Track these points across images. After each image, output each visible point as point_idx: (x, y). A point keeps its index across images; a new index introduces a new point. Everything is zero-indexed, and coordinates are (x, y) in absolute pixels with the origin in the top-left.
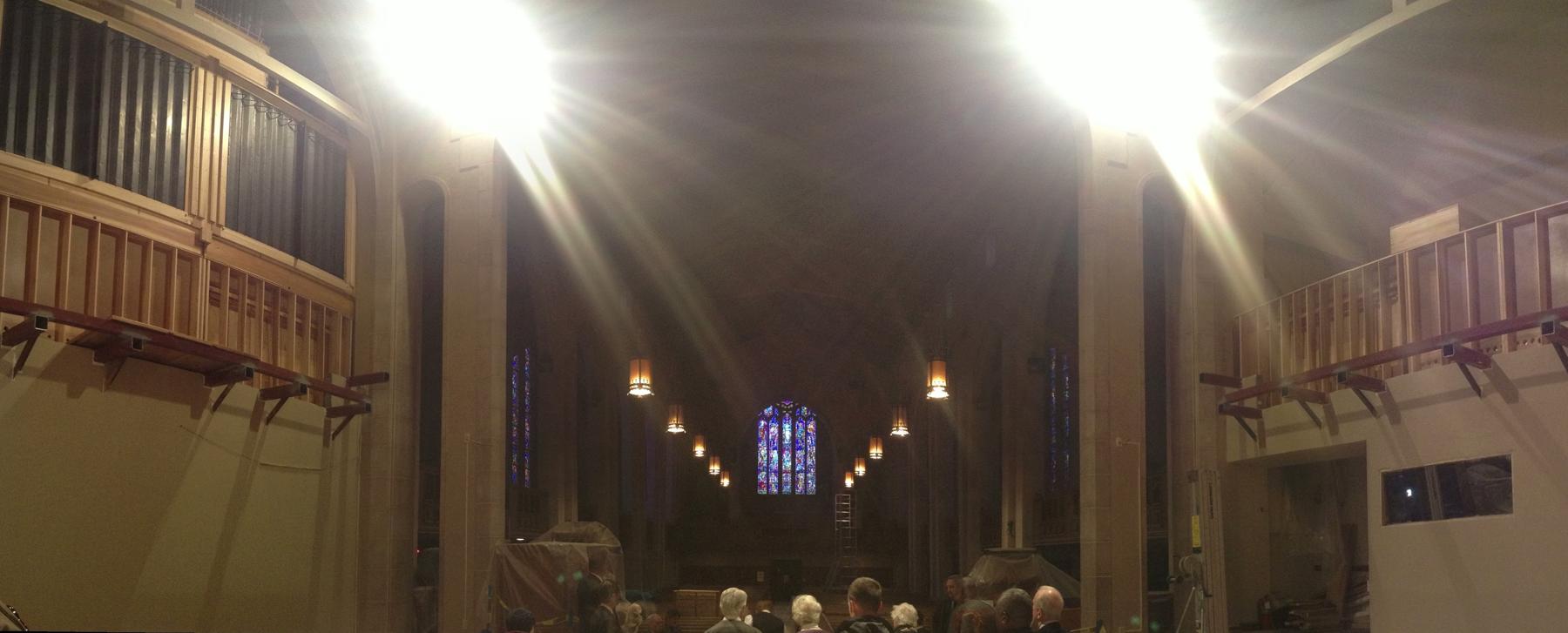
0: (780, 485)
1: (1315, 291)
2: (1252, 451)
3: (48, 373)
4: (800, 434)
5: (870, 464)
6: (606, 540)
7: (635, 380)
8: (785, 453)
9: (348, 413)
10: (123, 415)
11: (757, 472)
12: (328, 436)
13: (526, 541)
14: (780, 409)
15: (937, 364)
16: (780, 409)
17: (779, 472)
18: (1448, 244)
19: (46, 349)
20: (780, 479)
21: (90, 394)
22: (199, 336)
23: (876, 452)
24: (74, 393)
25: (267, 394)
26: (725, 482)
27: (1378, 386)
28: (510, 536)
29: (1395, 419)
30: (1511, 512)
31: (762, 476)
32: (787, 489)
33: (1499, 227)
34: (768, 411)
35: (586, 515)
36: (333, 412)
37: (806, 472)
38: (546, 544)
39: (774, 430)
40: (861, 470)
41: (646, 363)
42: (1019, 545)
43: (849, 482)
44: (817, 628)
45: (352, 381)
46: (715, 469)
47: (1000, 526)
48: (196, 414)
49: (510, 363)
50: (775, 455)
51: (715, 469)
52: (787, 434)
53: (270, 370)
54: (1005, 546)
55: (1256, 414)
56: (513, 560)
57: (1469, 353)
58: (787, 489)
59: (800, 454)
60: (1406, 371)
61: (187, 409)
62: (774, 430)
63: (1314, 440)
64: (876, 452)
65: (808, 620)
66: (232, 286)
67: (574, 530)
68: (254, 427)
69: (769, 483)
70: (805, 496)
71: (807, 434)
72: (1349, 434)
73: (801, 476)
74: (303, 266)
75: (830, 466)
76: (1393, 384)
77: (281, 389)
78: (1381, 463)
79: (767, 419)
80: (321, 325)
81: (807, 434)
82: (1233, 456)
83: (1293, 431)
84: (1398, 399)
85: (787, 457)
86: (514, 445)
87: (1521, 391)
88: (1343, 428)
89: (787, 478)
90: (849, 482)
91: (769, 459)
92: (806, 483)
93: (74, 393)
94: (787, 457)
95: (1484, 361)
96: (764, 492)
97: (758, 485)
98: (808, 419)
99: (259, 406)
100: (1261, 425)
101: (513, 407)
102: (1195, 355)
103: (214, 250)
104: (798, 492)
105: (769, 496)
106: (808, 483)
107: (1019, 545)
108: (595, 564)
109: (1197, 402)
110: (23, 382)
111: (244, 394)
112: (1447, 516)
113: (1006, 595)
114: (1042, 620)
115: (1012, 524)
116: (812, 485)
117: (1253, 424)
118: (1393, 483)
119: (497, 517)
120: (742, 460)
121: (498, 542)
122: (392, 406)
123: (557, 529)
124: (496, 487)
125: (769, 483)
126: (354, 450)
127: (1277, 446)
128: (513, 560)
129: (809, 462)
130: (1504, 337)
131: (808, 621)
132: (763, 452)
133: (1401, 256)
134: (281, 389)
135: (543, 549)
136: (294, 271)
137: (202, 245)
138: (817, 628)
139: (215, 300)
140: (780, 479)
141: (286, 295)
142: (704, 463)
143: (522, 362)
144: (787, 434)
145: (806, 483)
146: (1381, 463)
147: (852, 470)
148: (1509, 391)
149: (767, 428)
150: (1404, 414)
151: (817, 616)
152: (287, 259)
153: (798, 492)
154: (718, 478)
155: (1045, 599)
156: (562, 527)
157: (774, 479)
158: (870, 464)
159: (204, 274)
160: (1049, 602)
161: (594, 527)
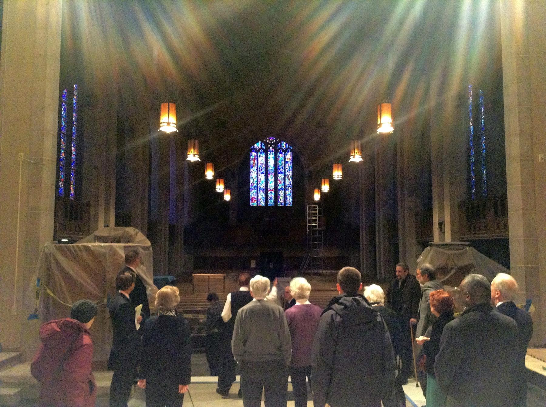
0: (266, 199)
4: (280, 162)
5: (332, 183)
6: (141, 240)
7: (164, 118)
8: (270, 177)
11: (249, 190)
13: (70, 242)
14: (266, 144)
16: (266, 144)
17: (266, 190)
20: (266, 194)
23: (337, 174)
26: (227, 197)
28: (56, 238)
31: (253, 193)
32: (271, 202)
34: (257, 145)
35: (123, 220)
37: (285, 190)
38: (90, 245)
39: (262, 160)
40: (326, 188)
41: (173, 107)
42: (448, 239)
43: (317, 197)
44: (308, 303)
46: (220, 188)
47: (431, 224)
49: (61, 96)
50: (262, 177)
51: (220, 188)
52: (271, 162)
54: (436, 239)
56: (60, 257)
58: (271, 202)
59: (280, 176)
62: (262, 160)
64: (337, 174)
65: (301, 296)
67: (113, 233)
69: (257, 198)
71: (286, 162)
73: (281, 193)
75: (302, 185)
79: (257, 151)
81: (286, 162)
85: (271, 178)
86: (63, 165)
89: (271, 194)
90: (317, 197)
91: (258, 181)
92: (285, 198)
94: (271, 178)
96: (255, 204)
98: (285, 151)
101: (64, 134)
104: (279, 204)
105: (258, 207)
106: (286, 198)
107: (448, 239)
108: (132, 257)
113: (467, 279)
114: (500, 299)
115: (441, 224)
116: (289, 200)
119: (46, 222)
120: (240, 181)
121: (47, 243)
123: (99, 233)
124: (47, 201)
125: (257, 198)
128: (60, 257)
129: (287, 183)
131: (301, 296)
132: (254, 174)
135: (87, 249)
138: (308, 303)
140: (266, 194)
142: (212, 184)
143: (71, 94)
144: (271, 162)
145: (285, 198)
147: (319, 188)
149: (257, 158)
151: (308, 293)
153: (279, 204)
154: (222, 194)
155: (503, 284)
156: (101, 231)
157: (262, 195)
158: (332, 183)
160: (507, 288)
161: (131, 230)
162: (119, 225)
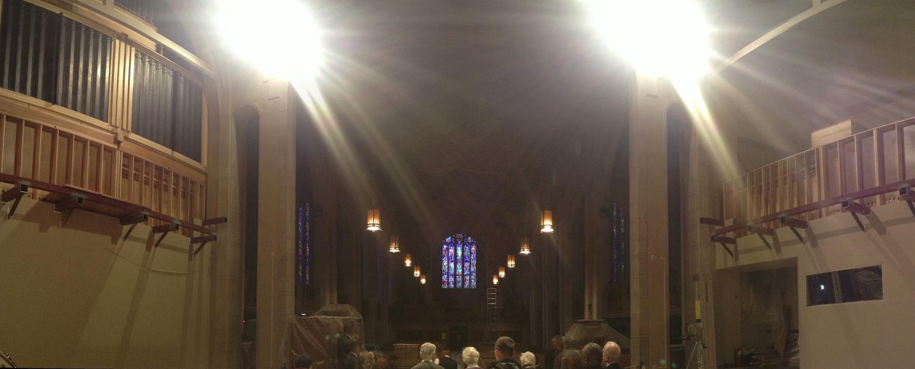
0: (455, 283)
1: (767, 169)
2: (731, 263)
3: (28, 217)
4: (467, 253)
5: (507, 270)
6: (354, 315)
7: (371, 221)
8: (458, 264)
9: (203, 241)
10: (72, 242)
11: (442, 275)
12: (192, 254)
13: (307, 315)
14: (455, 238)
15: (547, 212)
16: (455, 238)
17: (455, 275)
18: (845, 142)
19: (27, 203)
20: (455, 279)
21: (53, 230)
22: (116, 196)
23: (511, 264)
24: (43, 229)
25: (156, 230)
26: (423, 281)
27: (804, 225)
28: (297, 313)
29: (814, 244)
30: (882, 298)
31: (445, 278)
32: (459, 285)
33: (875, 133)
34: (448, 239)
35: (342, 300)
36: (194, 240)
37: (470, 275)
38: (319, 317)
39: (452, 251)
40: (502, 274)
42: (595, 318)
43: (495, 281)
44: (477, 366)
45: (205, 222)
46: (417, 273)
47: (583, 307)
48: (114, 242)
49: (297, 212)
50: (452, 265)
51: (417, 273)
52: (459, 253)
53: (157, 216)
54: (587, 318)
55: (733, 241)
56: (299, 327)
57: (857, 206)
58: (459, 285)
59: (467, 264)
60: (821, 216)
61: (109, 238)
62: (452, 251)
63: (767, 256)
64: (511, 264)
65: (471, 362)
66: (135, 166)
67: (335, 309)
68: (148, 249)
69: (449, 282)
70: (470, 289)
71: (471, 253)
72: (787, 253)
73: (468, 278)
74: (177, 155)
75: (484, 272)
76: (813, 224)
77: (164, 226)
78: (806, 270)
79: (448, 244)
80: (187, 190)
81: (471, 253)
82: (719, 266)
83: (755, 251)
84: (816, 232)
85: (459, 266)
86: (300, 260)
87: (888, 228)
88: (784, 249)
89: (459, 279)
90: (495, 281)
91: (449, 268)
92: (470, 282)
93: (43, 229)
94: (459, 266)
95: (866, 211)
96: (446, 287)
97: (442, 282)
98: (471, 244)
99: (151, 237)
100: (736, 248)
101: (299, 237)
102: (697, 207)
103: (125, 145)
104: (466, 287)
105: (449, 289)
106: (471, 282)
107: (595, 318)
108: (347, 329)
109: (698, 234)
110: (13, 223)
111: (143, 230)
112: (845, 301)
113: (587, 347)
114: (608, 361)
115: (590, 306)
116: (474, 283)
117: (731, 247)
118: (813, 281)
119: (290, 301)
120: (433, 268)
121: (291, 316)
122: (229, 236)
123: (325, 309)
124: (290, 284)
125: (449, 282)
126: (207, 262)
127: (745, 260)
128: (299, 327)
129: (472, 269)
130: (878, 197)
131: (472, 362)
132: (445, 263)
133: (818, 149)
134: (164, 226)
135: (317, 320)
136: (171, 158)
137: (118, 143)
138: (477, 366)
139: (125, 175)
140: (455, 279)
141: (167, 172)
142: (411, 270)
143: (305, 211)
144: (459, 253)
145: (470, 282)
146: (806, 270)
147: (497, 274)
148: (881, 228)
149: (448, 249)
150: (819, 241)
151: (477, 359)
152: (168, 151)
153: (466, 287)
154: (419, 278)
155: (610, 349)
156: (328, 307)
157: (451, 279)
158: (507, 270)
159: (119, 160)
160: (612, 351)
161: (347, 307)
162: (882, 294)
